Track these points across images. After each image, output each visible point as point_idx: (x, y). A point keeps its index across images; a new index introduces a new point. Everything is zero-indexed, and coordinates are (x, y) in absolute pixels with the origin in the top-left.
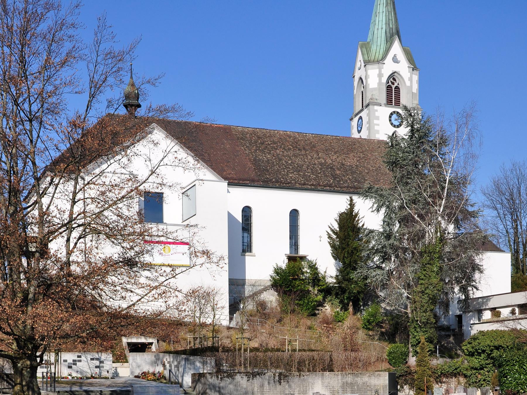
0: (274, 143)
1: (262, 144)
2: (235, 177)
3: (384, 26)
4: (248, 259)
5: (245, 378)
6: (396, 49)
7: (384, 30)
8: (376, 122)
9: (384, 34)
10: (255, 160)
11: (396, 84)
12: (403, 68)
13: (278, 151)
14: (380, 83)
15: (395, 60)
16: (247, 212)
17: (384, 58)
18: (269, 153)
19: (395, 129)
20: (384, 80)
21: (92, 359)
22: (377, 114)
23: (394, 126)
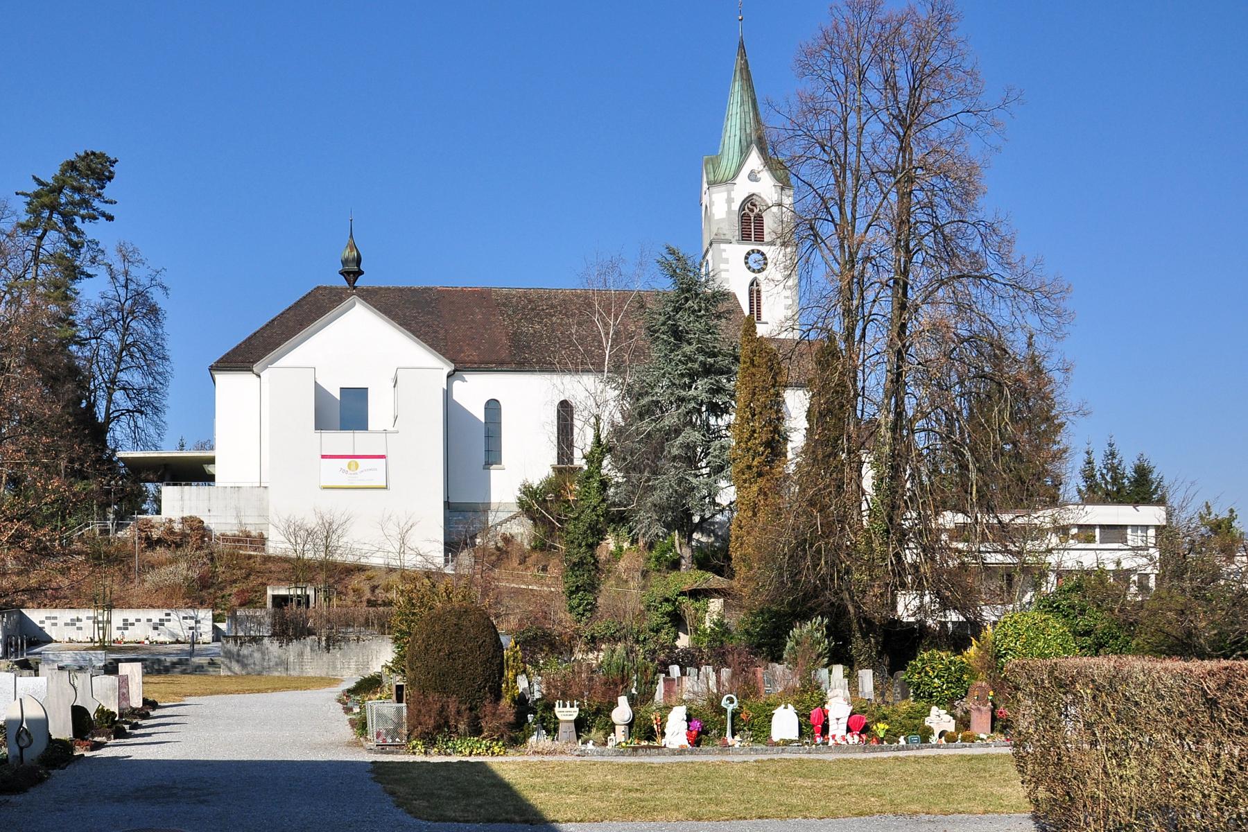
0: (552, 306)
1: (533, 309)
2: (476, 359)
3: (738, 133)
4: (495, 474)
5: (277, 644)
6: (754, 160)
7: (737, 138)
8: (722, 266)
9: (737, 143)
10: (515, 334)
11: (756, 211)
12: (767, 188)
13: (554, 319)
14: (729, 211)
15: (753, 177)
16: (493, 407)
17: (735, 176)
18: (539, 323)
19: (753, 275)
20: (736, 206)
21: (185, 618)
22: (724, 255)
23: (754, 271)
